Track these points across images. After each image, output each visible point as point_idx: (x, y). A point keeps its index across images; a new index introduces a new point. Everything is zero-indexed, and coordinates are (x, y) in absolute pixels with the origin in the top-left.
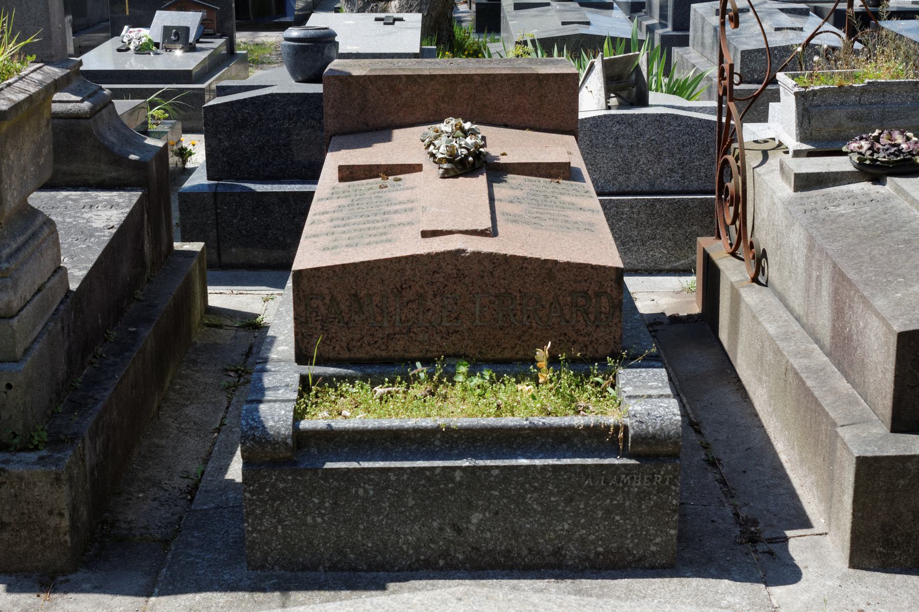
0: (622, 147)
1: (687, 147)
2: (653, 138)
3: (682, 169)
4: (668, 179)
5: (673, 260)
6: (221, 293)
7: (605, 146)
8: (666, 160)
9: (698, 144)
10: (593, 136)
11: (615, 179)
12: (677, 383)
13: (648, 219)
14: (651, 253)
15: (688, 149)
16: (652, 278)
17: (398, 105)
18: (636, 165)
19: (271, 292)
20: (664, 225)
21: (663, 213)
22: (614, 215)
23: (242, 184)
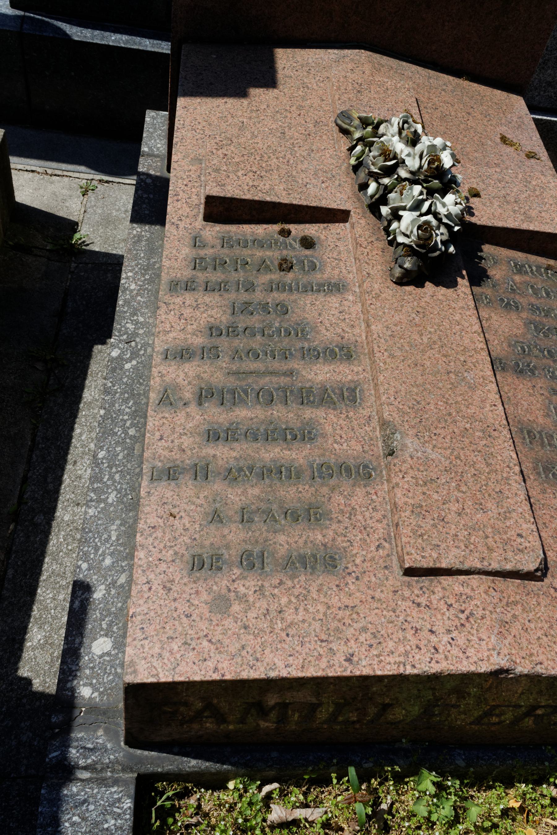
4: (542, 93)
6: (33, 171)
8: (549, 71)
19: (91, 177)
23: (56, 23)
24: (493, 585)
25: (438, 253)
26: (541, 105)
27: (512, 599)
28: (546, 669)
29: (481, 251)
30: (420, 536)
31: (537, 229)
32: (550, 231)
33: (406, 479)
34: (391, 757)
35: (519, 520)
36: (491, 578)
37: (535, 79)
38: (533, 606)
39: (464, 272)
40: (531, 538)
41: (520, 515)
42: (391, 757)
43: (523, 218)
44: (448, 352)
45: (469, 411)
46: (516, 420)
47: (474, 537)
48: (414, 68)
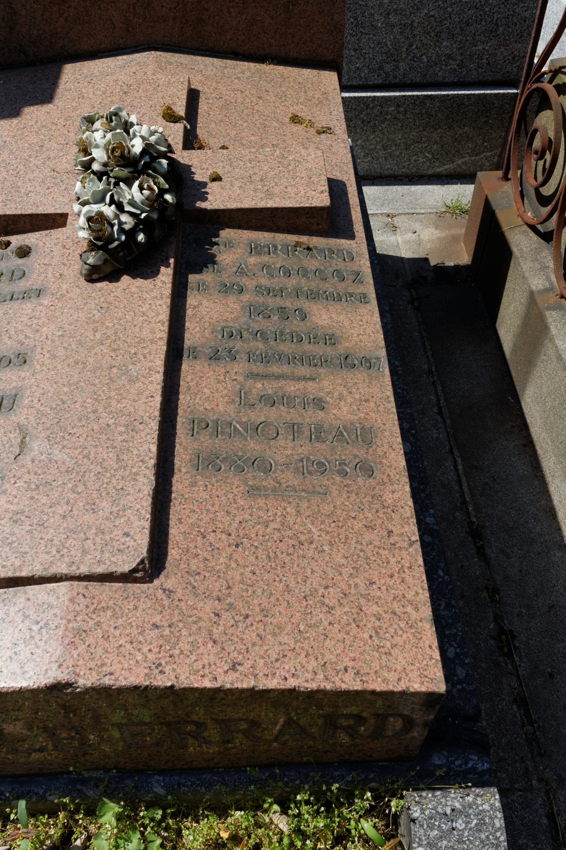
0: (392, 26)
1: (472, 25)
2: (432, 13)
3: (462, 54)
4: (444, 67)
5: (437, 165)
7: (372, 26)
8: (445, 43)
9: (486, 21)
10: (358, 12)
11: (381, 68)
12: (448, 422)
13: (415, 120)
14: (414, 158)
15: (472, 28)
16: (413, 188)
17: (66, 20)
18: (407, 49)
20: (433, 126)
21: (433, 113)
22: (377, 116)
24: (84, 591)
25: (116, 243)
26: (447, 80)
27: (103, 604)
28: (117, 680)
29: (218, 236)
30: (9, 543)
31: (275, 206)
32: (290, 205)
33: (17, 485)
34: (79, 787)
35: (132, 517)
36: (85, 583)
37: (432, 53)
38: (127, 611)
39: (172, 261)
40: (138, 537)
41: (135, 512)
42: (79, 787)
43: (263, 196)
44: (119, 346)
45: (119, 405)
46: (189, 410)
47: (71, 540)
48: (209, 60)
